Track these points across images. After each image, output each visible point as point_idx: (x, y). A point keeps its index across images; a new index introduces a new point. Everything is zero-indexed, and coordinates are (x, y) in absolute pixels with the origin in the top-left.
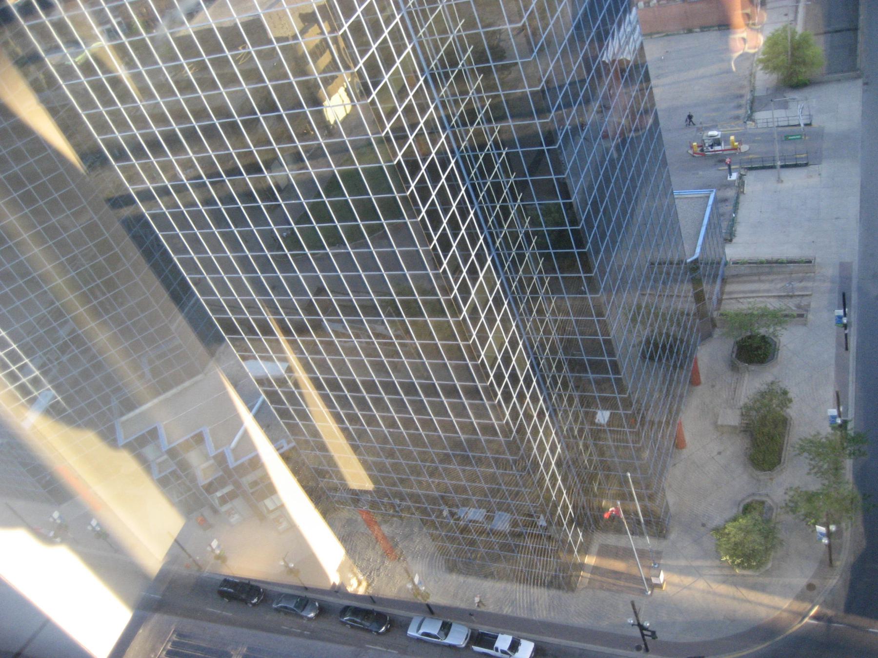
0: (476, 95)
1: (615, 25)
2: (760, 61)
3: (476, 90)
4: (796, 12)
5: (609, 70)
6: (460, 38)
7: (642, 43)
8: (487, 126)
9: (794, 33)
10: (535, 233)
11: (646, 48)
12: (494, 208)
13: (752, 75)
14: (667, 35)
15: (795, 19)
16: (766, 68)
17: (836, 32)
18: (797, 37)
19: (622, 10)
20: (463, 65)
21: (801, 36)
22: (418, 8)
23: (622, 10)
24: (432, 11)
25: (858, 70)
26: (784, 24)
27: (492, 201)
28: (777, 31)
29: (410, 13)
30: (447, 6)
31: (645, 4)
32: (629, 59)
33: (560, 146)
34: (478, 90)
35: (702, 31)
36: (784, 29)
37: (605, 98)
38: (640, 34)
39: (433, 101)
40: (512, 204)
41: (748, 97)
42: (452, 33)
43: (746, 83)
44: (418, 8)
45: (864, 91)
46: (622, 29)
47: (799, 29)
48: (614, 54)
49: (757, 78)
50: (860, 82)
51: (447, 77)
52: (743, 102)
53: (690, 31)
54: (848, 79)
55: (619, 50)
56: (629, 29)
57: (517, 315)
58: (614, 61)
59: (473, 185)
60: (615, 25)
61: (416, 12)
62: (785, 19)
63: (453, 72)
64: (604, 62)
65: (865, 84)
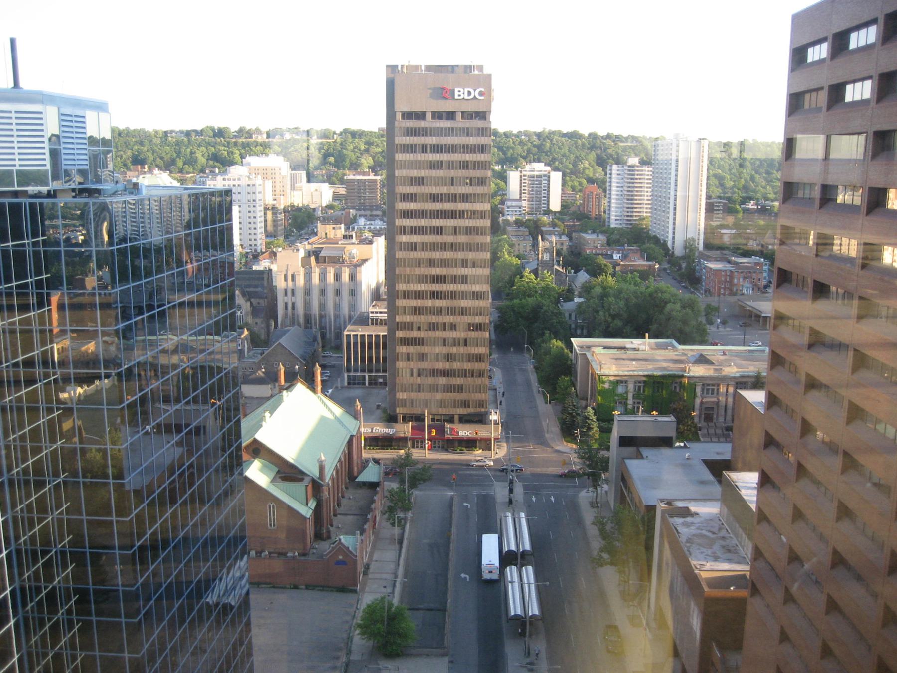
0: (65, 617)
1: (225, 571)
2: (359, 626)
3: (67, 610)
4: (394, 586)
5: (211, 612)
6: (60, 521)
7: (248, 593)
8: (42, 370)
9: (391, 605)
10: (76, 591)
11: (252, 596)
12: (45, 655)
13: (350, 639)
14: (274, 587)
15: (393, 592)
16: (362, 633)
17: (428, 610)
18: (393, 609)
19: (233, 556)
20: (59, 582)
21: (397, 607)
22: (26, 515)
23: (233, 556)
24: (40, 520)
25: (444, 648)
26: (382, 595)
27: (44, 646)
28: (376, 600)
29: (15, 519)
30: (58, 519)
31: (256, 553)
32: (233, 604)
33: (140, 620)
34: (69, 612)
35: (307, 588)
36: (383, 598)
37: (203, 640)
38: (247, 581)
39: (12, 581)
40: (48, 444)
41: (344, 659)
42: (52, 513)
43: (342, 645)
44: (26, 515)
45: (450, 668)
46: (231, 575)
47: (396, 601)
48: (219, 596)
49: (354, 641)
50: (446, 659)
51: (42, 624)
52: (339, 663)
53: (296, 587)
54: (436, 655)
55: (224, 594)
56: (238, 574)
57: (24, 645)
58: (217, 604)
59: (30, 654)
60: (225, 571)
61: (23, 518)
62: (384, 590)
63: (50, 620)
64: (208, 603)
65: (451, 662)
